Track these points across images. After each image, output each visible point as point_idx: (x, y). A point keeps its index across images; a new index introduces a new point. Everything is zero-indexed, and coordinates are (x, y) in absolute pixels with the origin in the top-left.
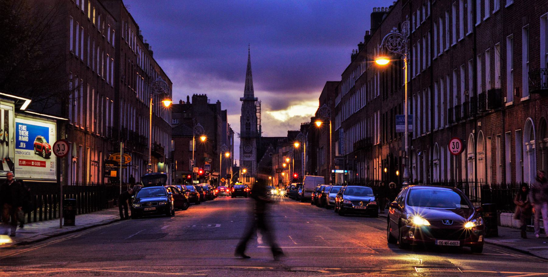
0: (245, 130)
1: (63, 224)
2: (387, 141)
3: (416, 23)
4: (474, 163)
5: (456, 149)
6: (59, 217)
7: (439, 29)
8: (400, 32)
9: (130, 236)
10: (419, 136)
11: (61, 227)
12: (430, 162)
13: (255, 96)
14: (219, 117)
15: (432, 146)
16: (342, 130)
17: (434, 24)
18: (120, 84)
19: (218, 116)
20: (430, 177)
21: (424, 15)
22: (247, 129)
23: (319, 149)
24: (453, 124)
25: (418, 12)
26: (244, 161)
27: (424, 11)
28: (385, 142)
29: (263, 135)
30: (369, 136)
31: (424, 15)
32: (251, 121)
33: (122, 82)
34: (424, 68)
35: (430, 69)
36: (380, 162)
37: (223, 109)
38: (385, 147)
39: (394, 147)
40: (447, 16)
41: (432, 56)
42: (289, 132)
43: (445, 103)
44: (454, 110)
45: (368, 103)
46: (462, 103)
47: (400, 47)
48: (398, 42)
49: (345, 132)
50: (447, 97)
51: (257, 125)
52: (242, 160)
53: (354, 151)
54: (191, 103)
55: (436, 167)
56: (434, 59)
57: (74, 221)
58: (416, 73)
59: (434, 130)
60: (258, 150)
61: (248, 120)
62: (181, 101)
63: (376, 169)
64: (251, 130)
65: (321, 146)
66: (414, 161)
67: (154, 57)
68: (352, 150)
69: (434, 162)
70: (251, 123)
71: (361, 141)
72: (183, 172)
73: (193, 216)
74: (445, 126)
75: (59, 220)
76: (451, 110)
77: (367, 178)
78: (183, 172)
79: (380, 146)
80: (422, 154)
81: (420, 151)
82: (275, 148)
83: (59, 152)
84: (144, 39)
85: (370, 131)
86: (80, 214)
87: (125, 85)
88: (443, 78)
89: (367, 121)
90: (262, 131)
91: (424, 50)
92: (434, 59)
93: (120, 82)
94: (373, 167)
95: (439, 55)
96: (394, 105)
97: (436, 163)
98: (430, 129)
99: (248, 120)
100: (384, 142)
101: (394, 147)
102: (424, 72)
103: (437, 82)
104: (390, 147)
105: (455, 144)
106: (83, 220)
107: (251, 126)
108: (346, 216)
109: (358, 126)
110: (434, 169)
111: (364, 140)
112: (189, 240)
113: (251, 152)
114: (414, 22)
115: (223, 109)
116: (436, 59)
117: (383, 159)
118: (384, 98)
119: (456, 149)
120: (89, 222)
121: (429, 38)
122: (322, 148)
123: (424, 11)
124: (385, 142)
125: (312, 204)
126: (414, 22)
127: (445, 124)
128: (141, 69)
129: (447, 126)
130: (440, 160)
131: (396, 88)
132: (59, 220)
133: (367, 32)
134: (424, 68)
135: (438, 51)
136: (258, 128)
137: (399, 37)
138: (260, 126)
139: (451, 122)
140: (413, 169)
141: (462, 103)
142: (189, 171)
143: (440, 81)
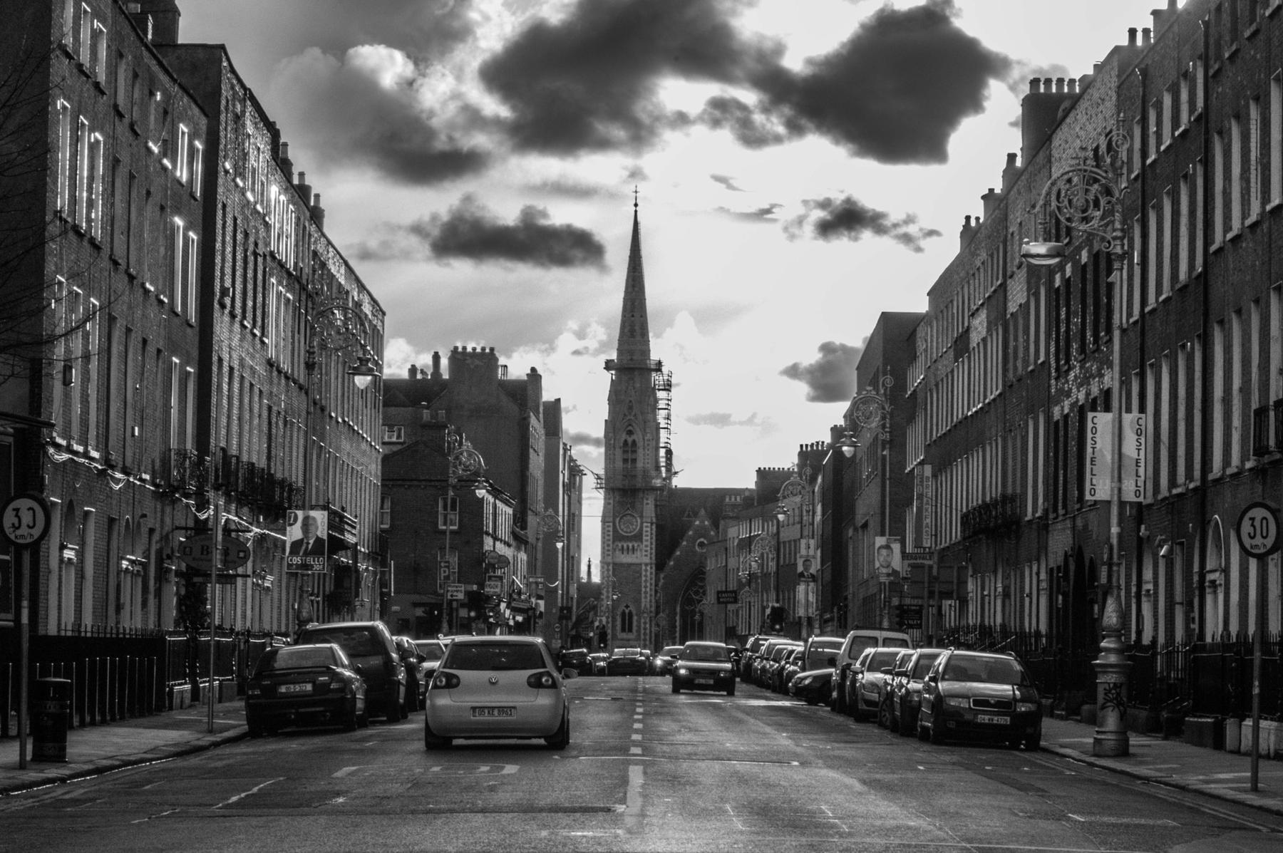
0: (619, 464)
1: (29, 758)
2: (1065, 507)
3: (1159, 135)
4: (1221, 597)
5: (1258, 540)
6: (19, 736)
7: (1231, 157)
8: (1098, 166)
9: (234, 799)
10: (1164, 492)
11: (22, 765)
12: (1196, 578)
13: (654, 356)
14: (536, 425)
15: (1203, 523)
16: (928, 470)
17: (1216, 138)
18: (217, 314)
19: (533, 420)
20: (1195, 626)
21: (1185, 108)
22: (625, 461)
23: (856, 529)
24: (1266, 459)
25: (1167, 101)
26: (615, 564)
27: (1184, 96)
28: (1061, 512)
29: (678, 482)
30: (1010, 491)
31: (1185, 108)
32: (638, 437)
33: (223, 306)
34: (1183, 275)
35: (1203, 281)
36: (1043, 576)
37: (547, 395)
38: (1059, 526)
39: (1086, 527)
40: (1254, 113)
41: (1208, 241)
42: (759, 471)
43: (1245, 390)
44: (1272, 414)
45: (1008, 386)
46: (1271, 403)
47: (1098, 213)
48: (1091, 197)
49: (935, 476)
50: (1250, 373)
51: (657, 448)
52: (609, 559)
53: (964, 539)
54: (446, 376)
55: (1215, 593)
56: (1213, 248)
57: (64, 749)
58: (1159, 291)
59: (1211, 477)
60: (661, 529)
61: (630, 433)
62: (413, 370)
63: (1030, 595)
64: (640, 464)
65: (860, 520)
66: (1148, 574)
67: (325, 230)
68: (956, 533)
69: (1210, 577)
70: (640, 444)
71: (985, 507)
72: (416, 598)
73: (988, 776)
74: (1243, 462)
75: (16, 746)
76: (1261, 413)
77: (1003, 626)
78: (416, 598)
79: (1043, 525)
80: (1171, 551)
81: (1165, 541)
82: (716, 525)
83: (19, 532)
84: (296, 171)
85: (1014, 474)
86: (83, 725)
87: (233, 316)
88: (1239, 312)
89: (1005, 440)
90: (676, 466)
91: (1184, 221)
92: (1213, 248)
93: (216, 306)
94: (1022, 589)
95: (1229, 236)
96: (1088, 394)
97: (1213, 582)
98: (1197, 473)
99: (630, 433)
100: (1055, 510)
101: (1086, 527)
102: (1180, 290)
103: (1221, 322)
104: (1074, 527)
105: (1257, 523)
106: (92, 745)
107: (640, 451)
108: (946, 744)
109: (976, 461)
110: (1209, 599)
111: (995, 503)
112: (413, 812)
113: (638, 537)
114: (1153, 129)
115: (547, 395)
116: (1220, 250)
117: (1052, 565)
118: (1057, 369)
119: (1258, 540)
120: (110, 751)
121: (1200, 182)
122: (865, 526)
123: (1184, 96)
124: (1061, 512)
125: (833, 710)
126: (1153, 129)
127: (1244, 458)
128: (282, 265)
129: (1248, 465)
130: (1226, 571)
131: (1096, 340)
132: (16, 746)
133: (1012, 157)
134: (1183, 275)
135: (1227, 228)
136: (663, 461)
137: (1096, 181)
138: (669, 453)
139: (1261, 450)
140: (1144, 599)
141: (1271, 403)
142: (435, 593)
143: (1230, 321)
